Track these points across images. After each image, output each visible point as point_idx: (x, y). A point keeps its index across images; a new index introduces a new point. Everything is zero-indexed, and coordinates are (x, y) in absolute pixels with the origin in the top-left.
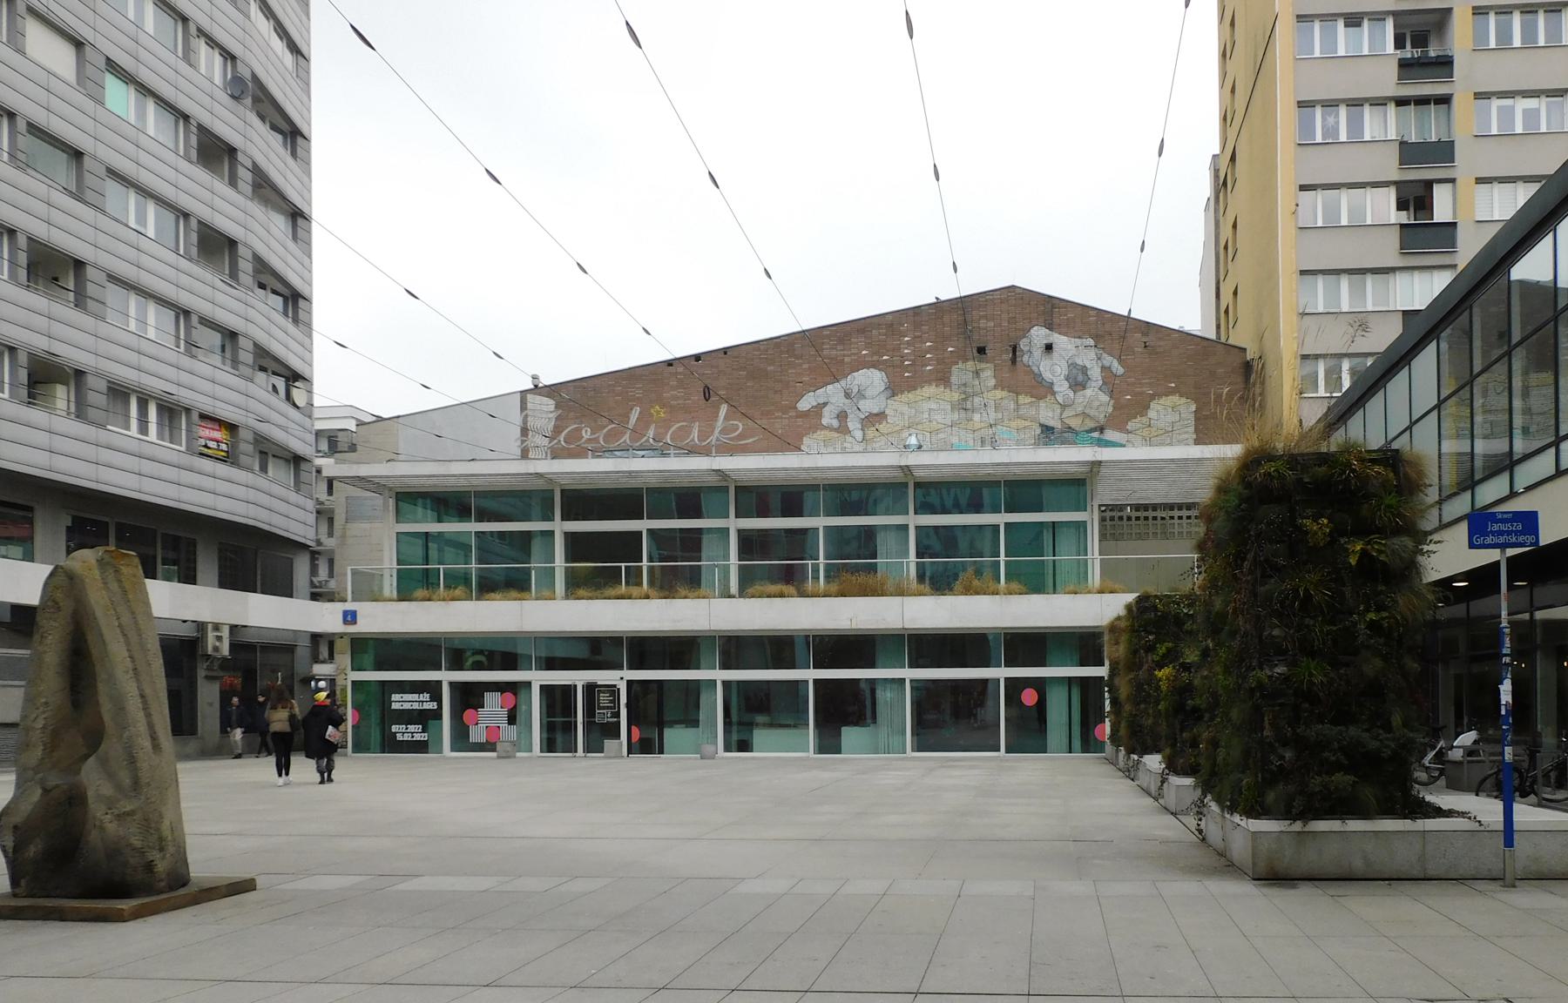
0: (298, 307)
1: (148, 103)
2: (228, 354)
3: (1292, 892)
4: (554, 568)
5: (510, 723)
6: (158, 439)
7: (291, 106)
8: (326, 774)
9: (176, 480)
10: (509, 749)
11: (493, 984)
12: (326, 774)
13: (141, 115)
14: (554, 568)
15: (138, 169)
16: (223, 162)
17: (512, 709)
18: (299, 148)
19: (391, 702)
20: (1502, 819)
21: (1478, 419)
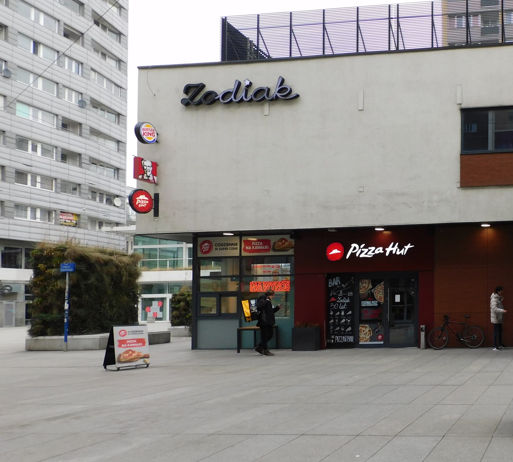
0: (119, 172)
1: (39, 112)
2: (81, 11)
3: (463, 190)
4: (182, 260)
5: (160, 311)
6: (31, 219)
7: (116, 24)
8: (149, 364)
9: (9, 159)
10: (151, 320)
11: (297, 436)
12: (149, 364)
13: (35, 117)
14: (182, 260)
15: (12, 58)
16: (78, 128)
17: (161, 306)
18: (122, 39)
19: (291, 266)
20: (223, 275)
21: (499, 25)
